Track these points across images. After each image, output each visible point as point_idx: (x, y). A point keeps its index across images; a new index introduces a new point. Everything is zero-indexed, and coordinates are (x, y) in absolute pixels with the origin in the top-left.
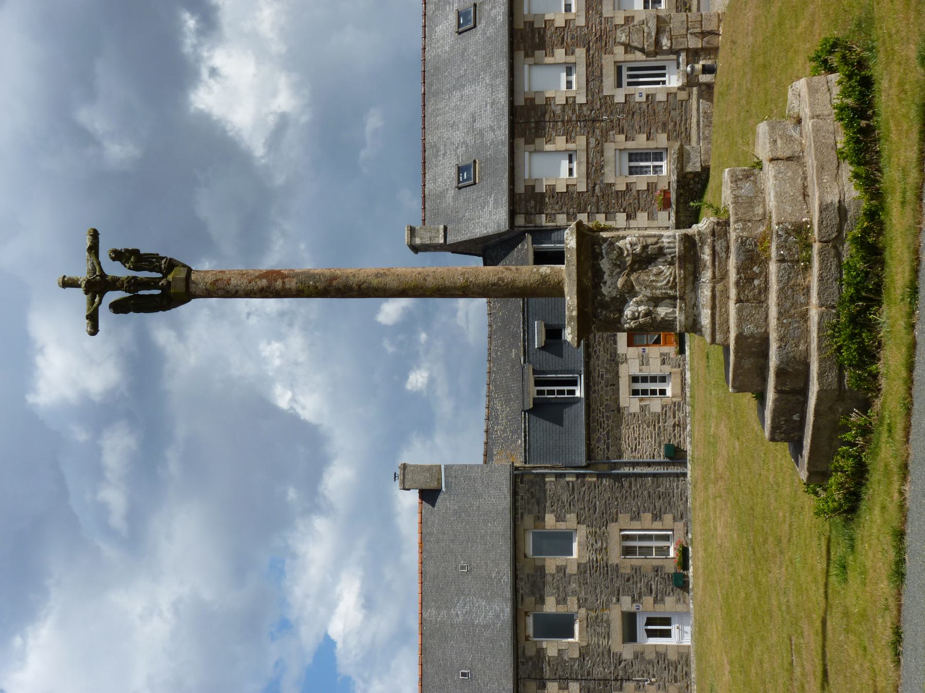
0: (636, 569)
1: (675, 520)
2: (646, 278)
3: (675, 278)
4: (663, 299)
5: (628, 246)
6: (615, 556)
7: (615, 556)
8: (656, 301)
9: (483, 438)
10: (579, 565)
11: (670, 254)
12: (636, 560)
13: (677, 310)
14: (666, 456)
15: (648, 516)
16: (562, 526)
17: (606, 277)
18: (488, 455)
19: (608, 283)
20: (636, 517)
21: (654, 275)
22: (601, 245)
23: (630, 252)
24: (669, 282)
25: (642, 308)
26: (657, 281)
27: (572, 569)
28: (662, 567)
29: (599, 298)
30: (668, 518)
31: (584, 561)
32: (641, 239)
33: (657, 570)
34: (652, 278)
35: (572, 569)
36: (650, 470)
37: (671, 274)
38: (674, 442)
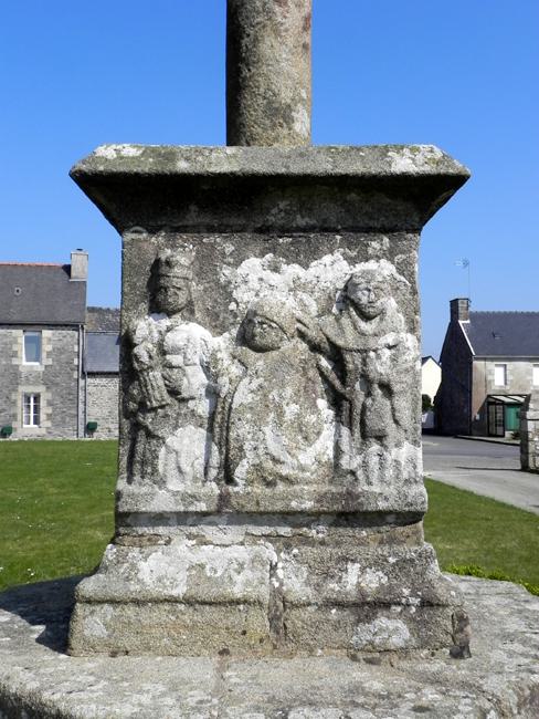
0: (14, 403)
1: (48, 428)
2: (289, 391)
3: (286, 479)
4: (224, 443)
5: (390, 339)
6: (23, 389)
7: (23, 389)
8: (219, 425)
9: (104, 307)
10: (17, 366)
11: (365, 465)
12: (20, 402)
13: (186, 486)
14: (89, 423)
15: (50, 411)
16: (44, 355)
17: (293, 270)
18: (92, 310)
19: (274, 278)
20: (50, 404)
21: (299, 416)
22: (390, 255)
23: (372, 343)
24: (276, 461)
25: (195, 381)
26: (279, 422)
27: (15, 362)
28: (16, 420)
29: (229, 248)
30: (49, 424)
31: (20, 369)
32: (408, 379)
33: (14, 416)
34: (291, 410)
35: (15, 362)
36: (80, 413)
37: (302, 469)
38: (98, 428)
